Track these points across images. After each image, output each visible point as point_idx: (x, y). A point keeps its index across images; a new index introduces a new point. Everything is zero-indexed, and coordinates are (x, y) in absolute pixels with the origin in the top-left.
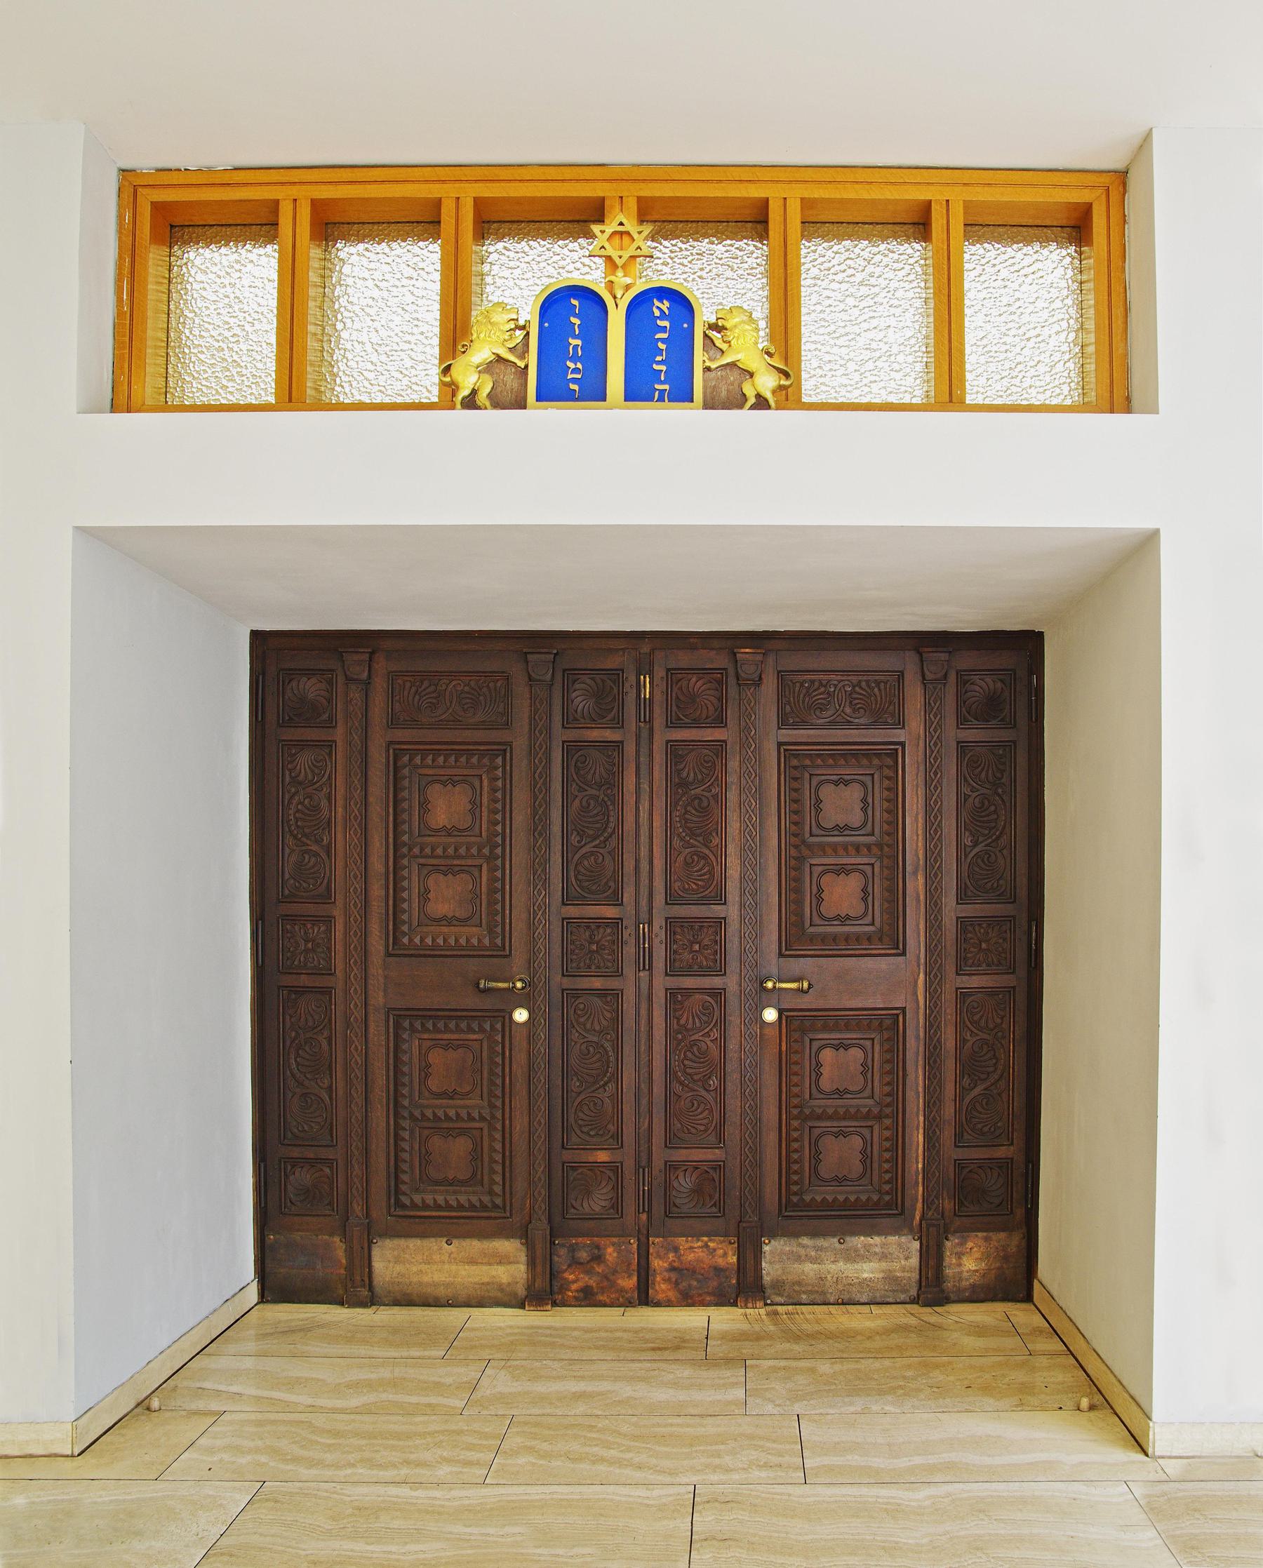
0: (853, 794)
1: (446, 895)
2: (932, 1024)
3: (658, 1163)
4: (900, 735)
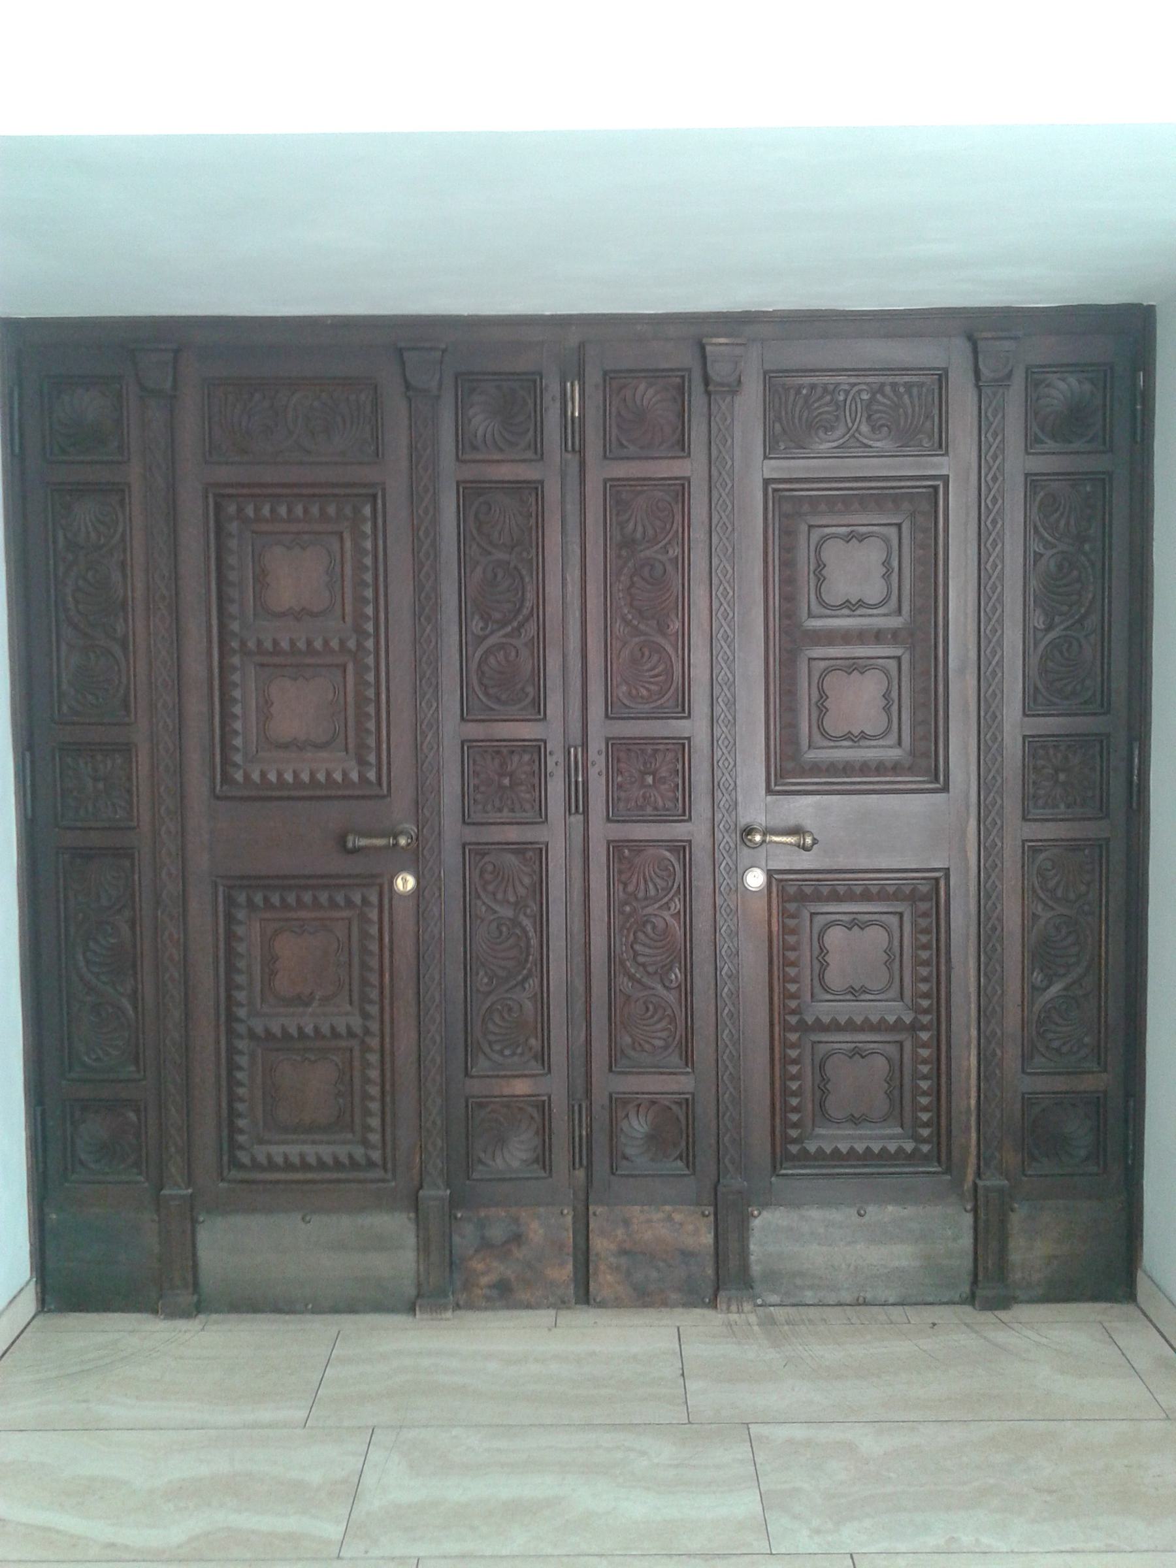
0: (871, 555)
1: (297, 709)
2: (986, 895)
3: (600, 1097)
4: (942, 465)
